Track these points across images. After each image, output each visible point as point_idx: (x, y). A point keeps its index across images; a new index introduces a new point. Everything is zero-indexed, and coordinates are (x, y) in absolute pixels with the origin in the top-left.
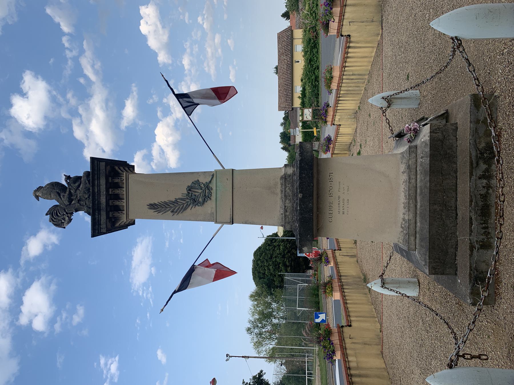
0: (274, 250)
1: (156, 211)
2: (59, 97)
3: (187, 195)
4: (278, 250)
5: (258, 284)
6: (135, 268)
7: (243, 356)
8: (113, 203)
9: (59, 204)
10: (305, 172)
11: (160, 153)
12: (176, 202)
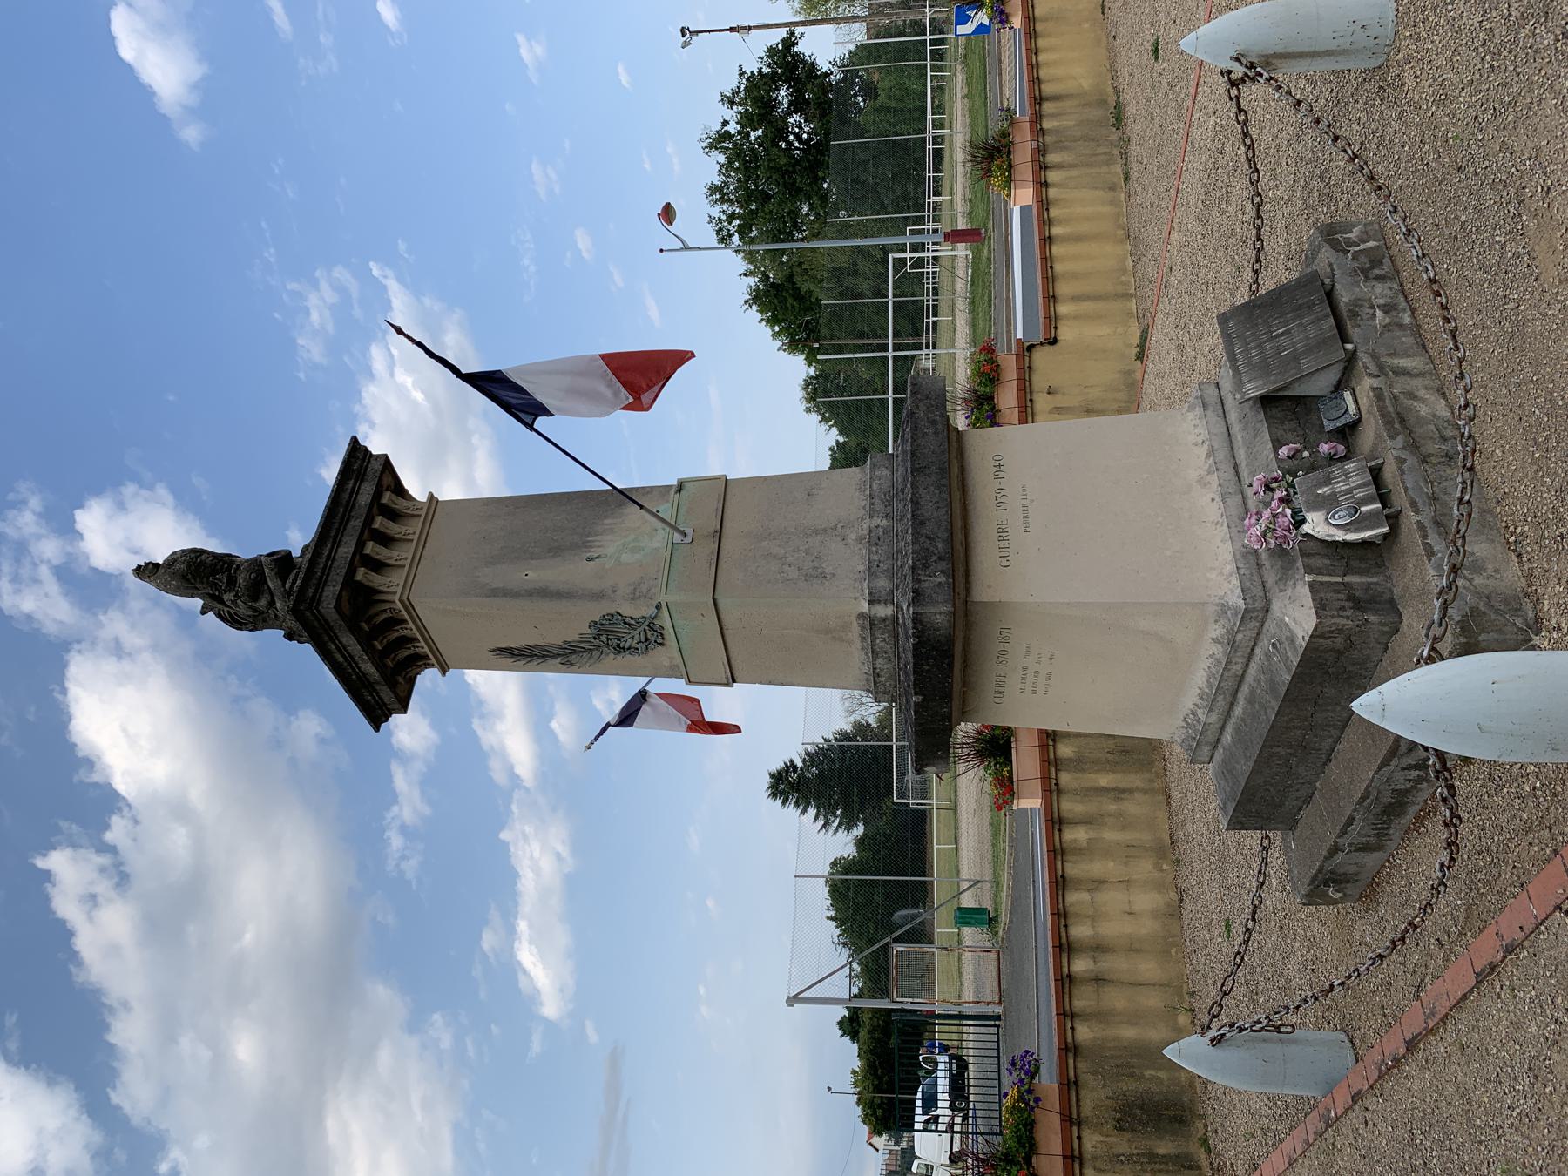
7: (731, 28)
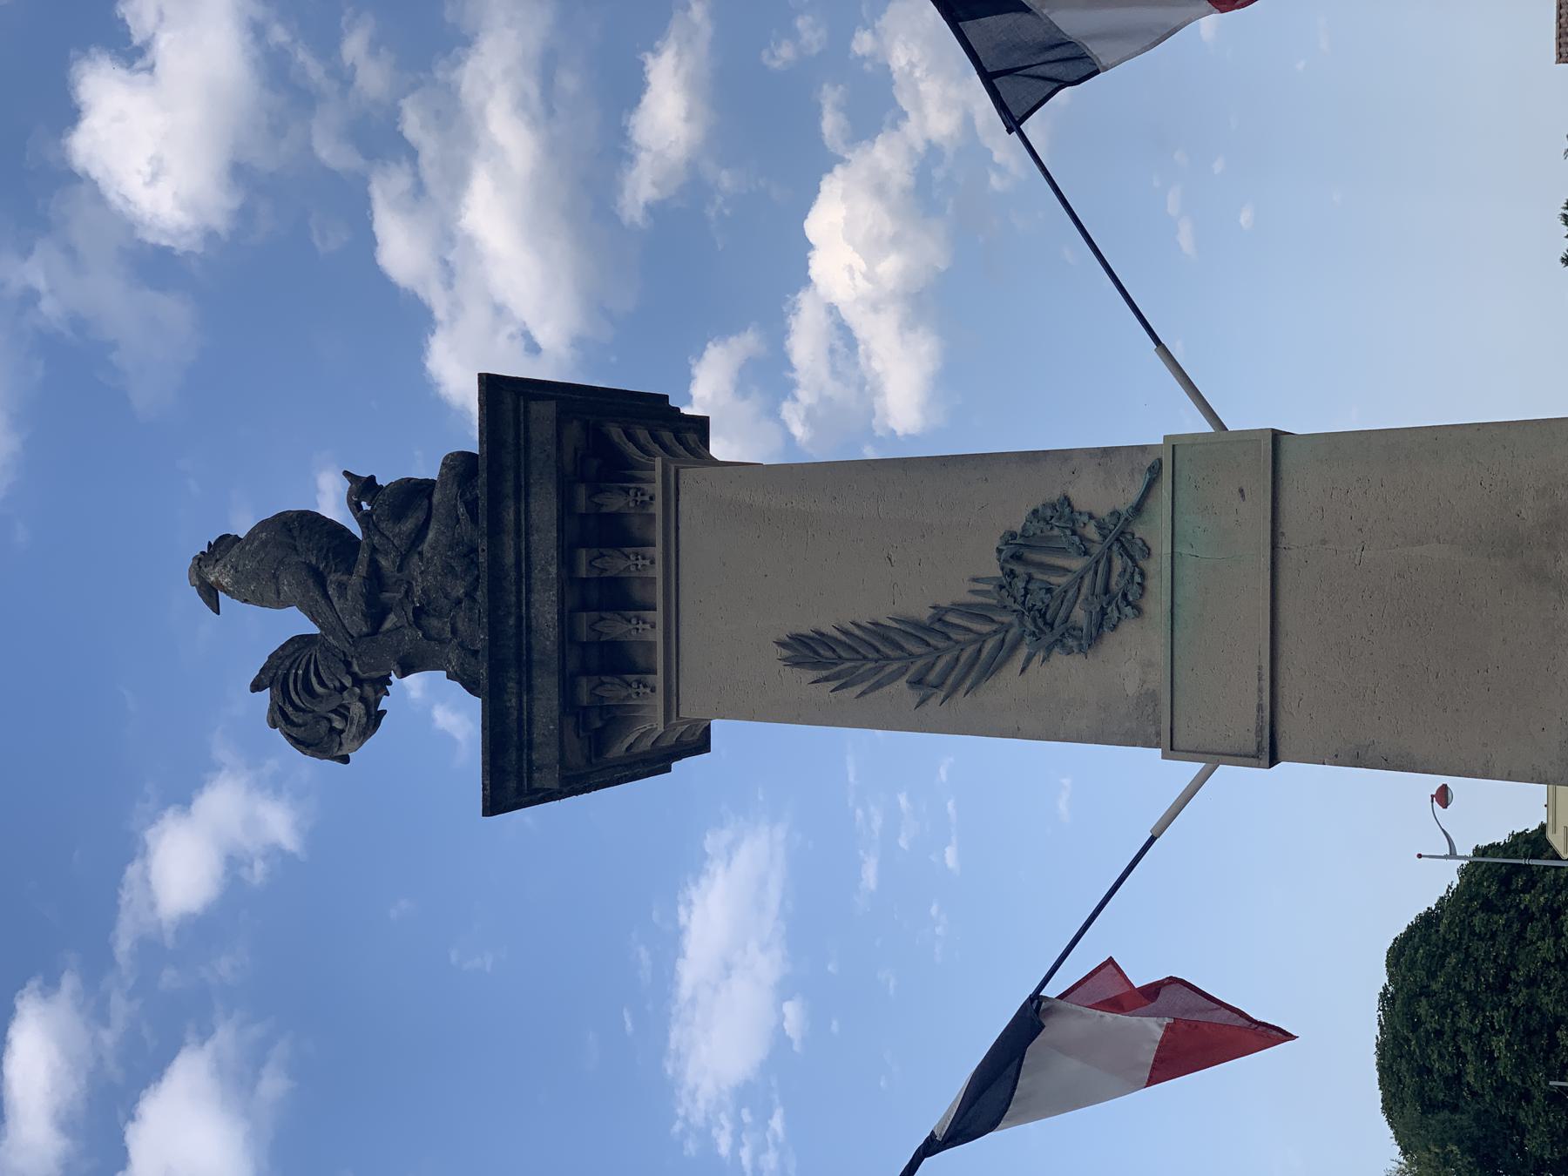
0: (1521, 935)
1: (826, 679)
2: (302, 56)
3: (1002, 587)
4: (1550, 941)
6: (693, 1001)
8: (598, 627)
9: (315, 630)
11: (832, 351)
12: (937, 626)
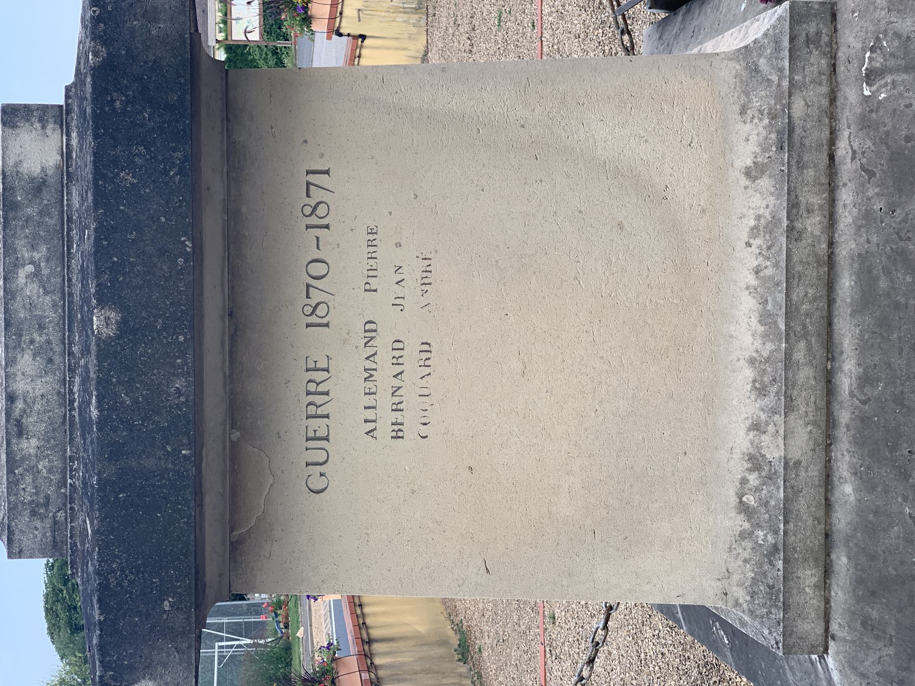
5: (67, 652)
10: (139, 155)
